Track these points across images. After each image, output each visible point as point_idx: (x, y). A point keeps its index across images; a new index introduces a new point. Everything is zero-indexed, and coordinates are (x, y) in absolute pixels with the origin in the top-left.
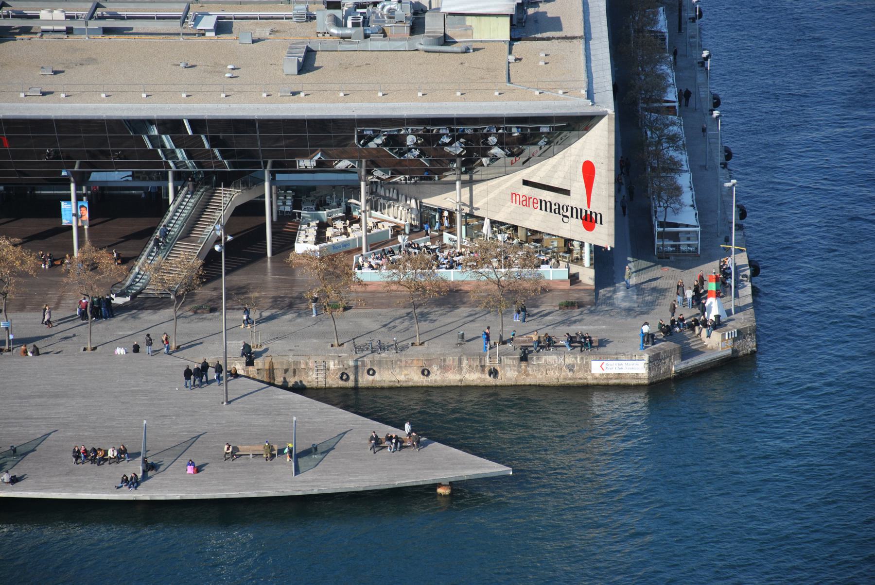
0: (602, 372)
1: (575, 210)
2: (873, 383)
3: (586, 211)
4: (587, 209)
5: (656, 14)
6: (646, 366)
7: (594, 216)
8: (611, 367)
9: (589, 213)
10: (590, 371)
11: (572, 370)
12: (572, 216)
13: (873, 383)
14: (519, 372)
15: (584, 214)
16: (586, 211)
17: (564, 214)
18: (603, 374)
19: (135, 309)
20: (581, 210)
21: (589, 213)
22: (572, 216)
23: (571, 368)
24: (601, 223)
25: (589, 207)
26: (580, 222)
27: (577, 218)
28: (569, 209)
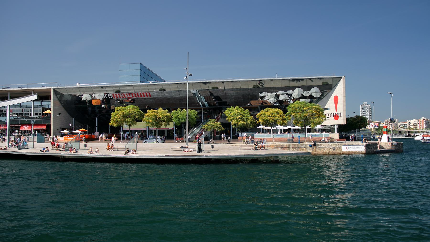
0: (346, 150)
1: (331, 114)
2: (0, 180)
3: (335, 113)
4: (336, 113)
5: (299, 126)
6: (365, 148)
7: (338, 114)
8: (350, 148)
9: (336, 114)
10: (342, 150)
11: (334, 150)
12: (330, 117)
13: (0, 180)
14: (313, 150)
15: (334, 115)
16: (335, 113)
17: (327, 117)
18: (347, 151)
19: (276, 215)
20: (333, 113)
21: (336, 114)
22: (330, 117)
23: (334, 148)
24: (341, 116)
25: (336, 112)
26: (333, 118)
27: (332, 117)
28: (329, 114)
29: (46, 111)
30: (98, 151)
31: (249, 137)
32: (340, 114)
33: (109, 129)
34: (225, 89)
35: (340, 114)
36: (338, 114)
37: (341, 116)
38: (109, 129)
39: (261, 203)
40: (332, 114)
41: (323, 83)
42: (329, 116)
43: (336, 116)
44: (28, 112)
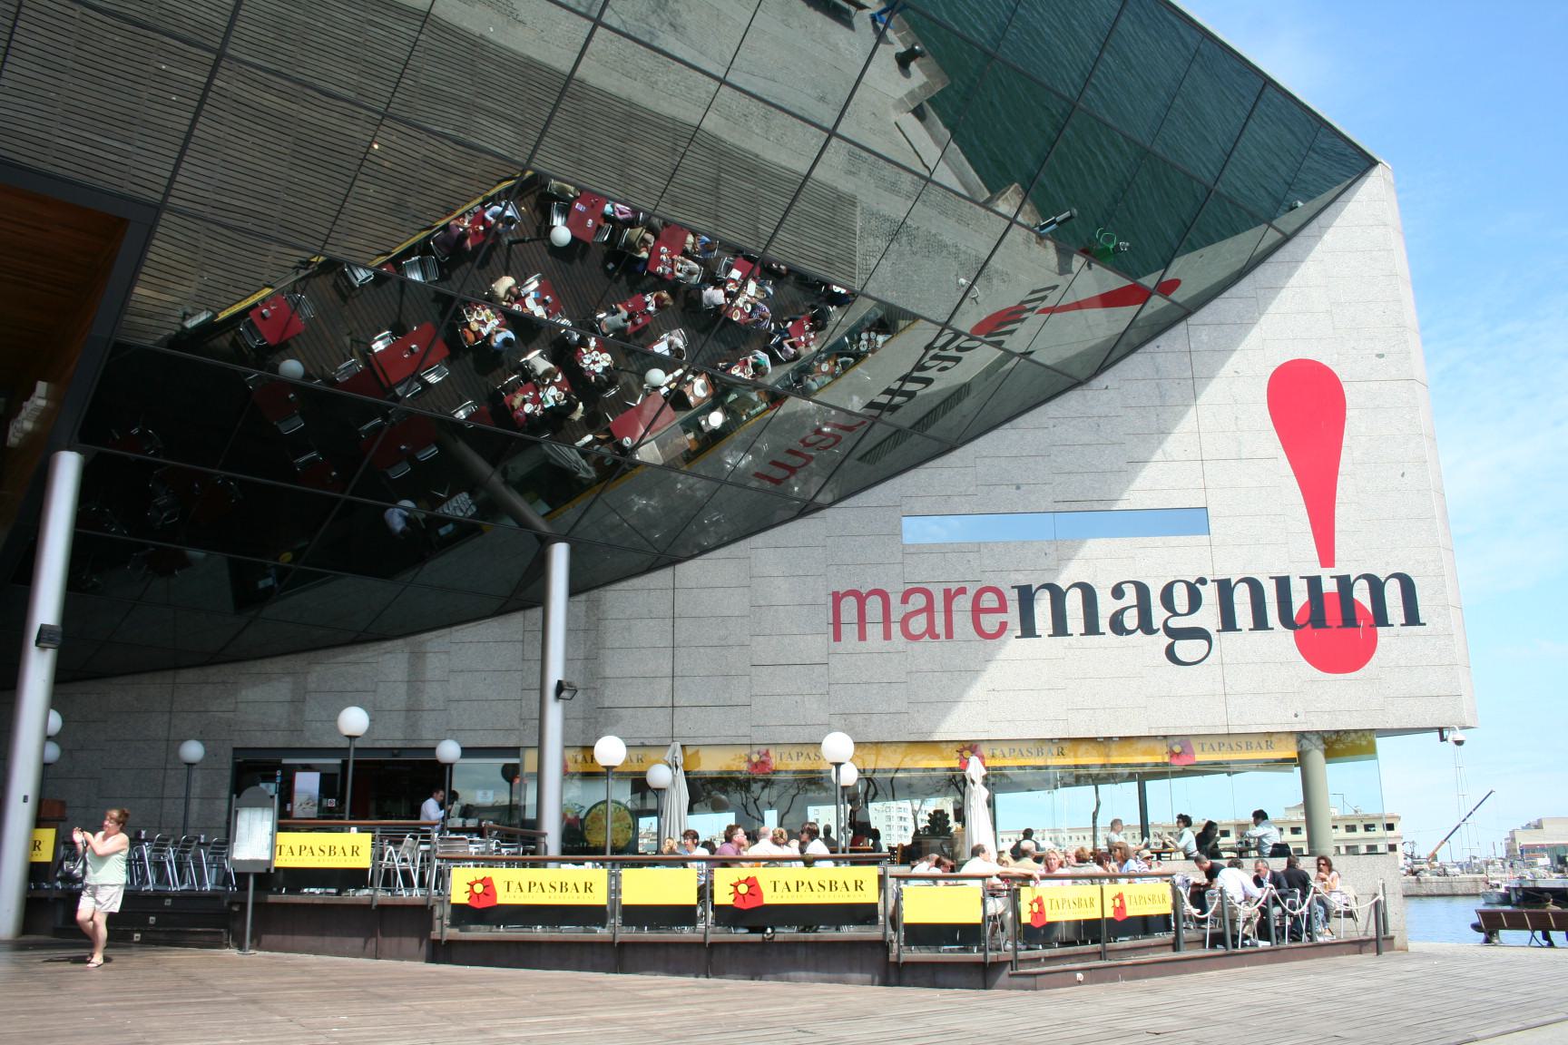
4: (1315, 570)
7: (1362, 594)
9: (1329, 586)
12: (1228, 623)
15: (1300, 597)
16: (1314, 583)
17: (1175, 623)
21: (1329, 586)
22: (1228, 623)
24: (1412, 617)
25: (1327, 557)
27: (1260, 622)
28: (1210, 594)
29: (918, 70)
30: (1178, 754)
31: (268, 576)
32: (1393, 593)
33: (47, 606)
34: (429, 12)
35: (1393, 593)
36: (1362, 594)
37: (1412, 617)
38: (47, 606)
39: (28, 425)
40: (1255, 587)
41: (474, 7)
42: (1208, 616)
43: (1333, 613)
44: (578, 844)
